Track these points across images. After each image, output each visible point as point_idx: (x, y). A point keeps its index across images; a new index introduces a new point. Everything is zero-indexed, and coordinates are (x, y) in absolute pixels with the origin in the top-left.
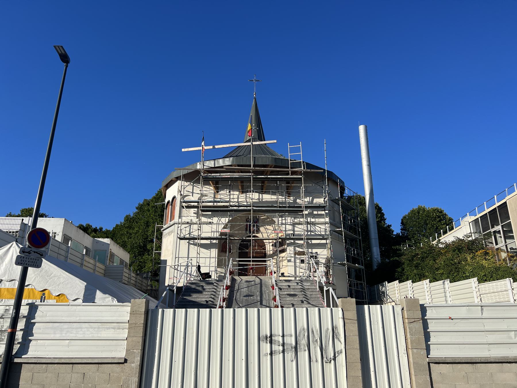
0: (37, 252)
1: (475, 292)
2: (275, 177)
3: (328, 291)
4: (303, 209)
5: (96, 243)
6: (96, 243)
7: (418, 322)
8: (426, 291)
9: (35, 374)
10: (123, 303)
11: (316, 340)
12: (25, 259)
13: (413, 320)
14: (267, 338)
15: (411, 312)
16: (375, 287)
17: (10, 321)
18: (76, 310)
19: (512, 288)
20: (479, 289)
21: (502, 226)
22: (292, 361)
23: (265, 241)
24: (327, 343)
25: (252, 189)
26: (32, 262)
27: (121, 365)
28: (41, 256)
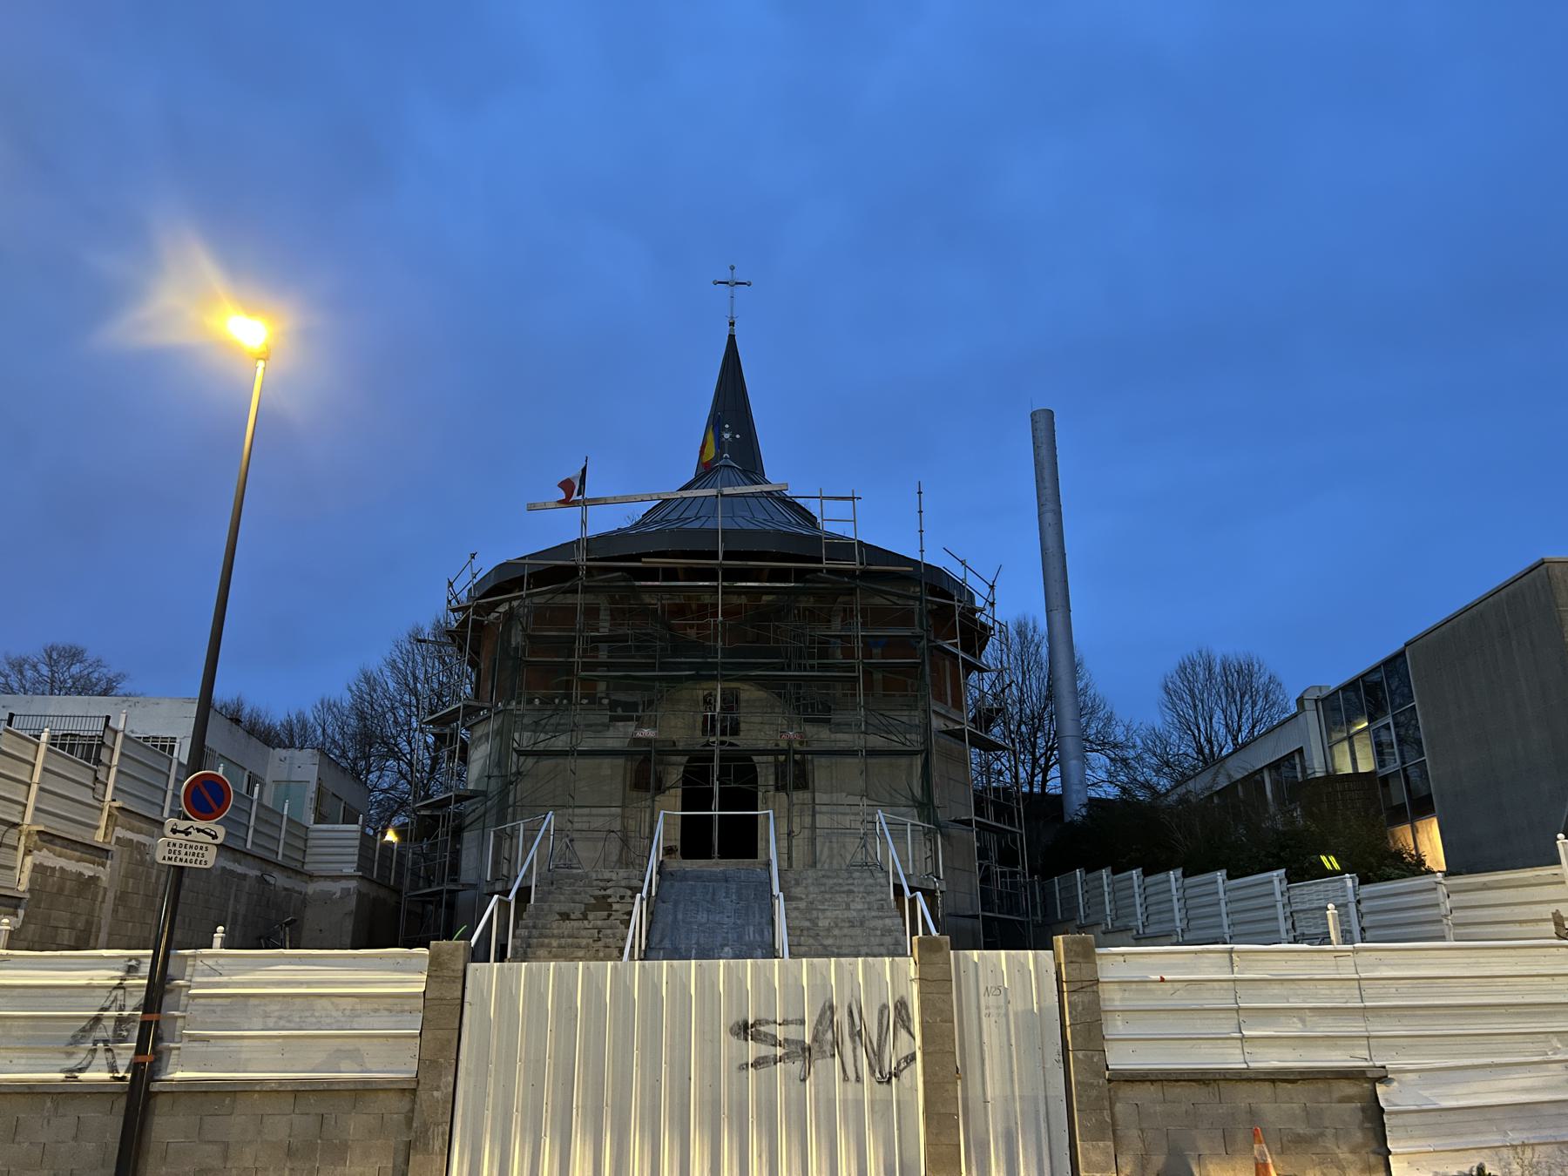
0: (203, 831)
1: (1279, 905)
2: (783, 585)
3: (913, 901)
4: (856, 674)
5: (281, 760)
6: (281, 760)
7: (1089, 989)
8: (1175, 899)
9: (205, 1118)
10: (410, 948)
11: (858, 1032)
12: (177, 848)
13: (1079, 985)
14: (748, 1028)
15: (1075, 966)
16: (1075, 874)
17: (144, 993)
18: (191, 944)
19: (1358, 898)
20: (1289, 897)
21: (1393, 716)
22: (801, 1080)
23: (755, 758)
24: (883, 1038)
25: (720, 618)
26: (193, 855)
27: (1520, 889)
28: (213, 839)
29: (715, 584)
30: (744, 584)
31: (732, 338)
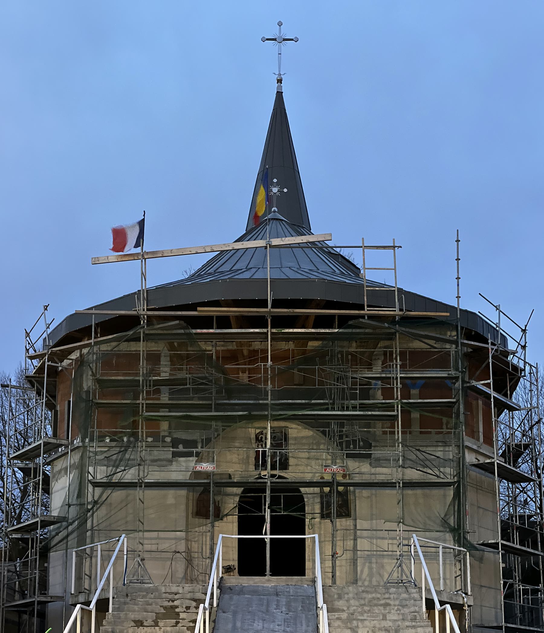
29: (265, 330)
30: (291, 330)
31: (279, 95)
